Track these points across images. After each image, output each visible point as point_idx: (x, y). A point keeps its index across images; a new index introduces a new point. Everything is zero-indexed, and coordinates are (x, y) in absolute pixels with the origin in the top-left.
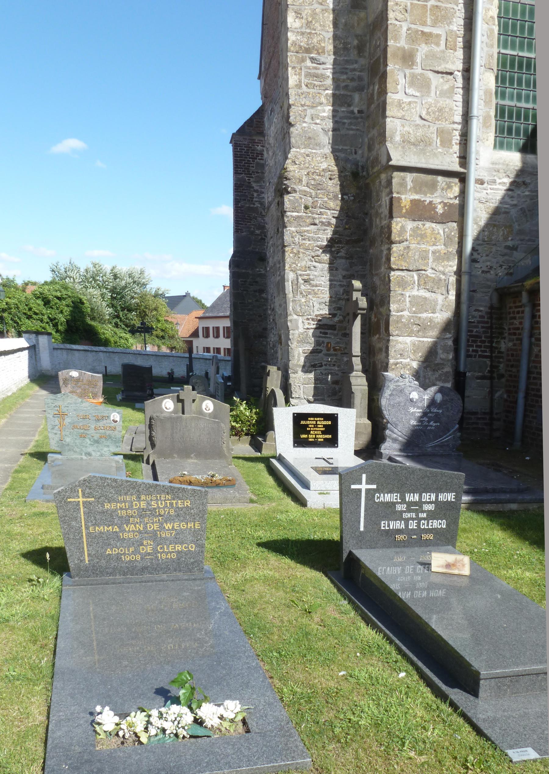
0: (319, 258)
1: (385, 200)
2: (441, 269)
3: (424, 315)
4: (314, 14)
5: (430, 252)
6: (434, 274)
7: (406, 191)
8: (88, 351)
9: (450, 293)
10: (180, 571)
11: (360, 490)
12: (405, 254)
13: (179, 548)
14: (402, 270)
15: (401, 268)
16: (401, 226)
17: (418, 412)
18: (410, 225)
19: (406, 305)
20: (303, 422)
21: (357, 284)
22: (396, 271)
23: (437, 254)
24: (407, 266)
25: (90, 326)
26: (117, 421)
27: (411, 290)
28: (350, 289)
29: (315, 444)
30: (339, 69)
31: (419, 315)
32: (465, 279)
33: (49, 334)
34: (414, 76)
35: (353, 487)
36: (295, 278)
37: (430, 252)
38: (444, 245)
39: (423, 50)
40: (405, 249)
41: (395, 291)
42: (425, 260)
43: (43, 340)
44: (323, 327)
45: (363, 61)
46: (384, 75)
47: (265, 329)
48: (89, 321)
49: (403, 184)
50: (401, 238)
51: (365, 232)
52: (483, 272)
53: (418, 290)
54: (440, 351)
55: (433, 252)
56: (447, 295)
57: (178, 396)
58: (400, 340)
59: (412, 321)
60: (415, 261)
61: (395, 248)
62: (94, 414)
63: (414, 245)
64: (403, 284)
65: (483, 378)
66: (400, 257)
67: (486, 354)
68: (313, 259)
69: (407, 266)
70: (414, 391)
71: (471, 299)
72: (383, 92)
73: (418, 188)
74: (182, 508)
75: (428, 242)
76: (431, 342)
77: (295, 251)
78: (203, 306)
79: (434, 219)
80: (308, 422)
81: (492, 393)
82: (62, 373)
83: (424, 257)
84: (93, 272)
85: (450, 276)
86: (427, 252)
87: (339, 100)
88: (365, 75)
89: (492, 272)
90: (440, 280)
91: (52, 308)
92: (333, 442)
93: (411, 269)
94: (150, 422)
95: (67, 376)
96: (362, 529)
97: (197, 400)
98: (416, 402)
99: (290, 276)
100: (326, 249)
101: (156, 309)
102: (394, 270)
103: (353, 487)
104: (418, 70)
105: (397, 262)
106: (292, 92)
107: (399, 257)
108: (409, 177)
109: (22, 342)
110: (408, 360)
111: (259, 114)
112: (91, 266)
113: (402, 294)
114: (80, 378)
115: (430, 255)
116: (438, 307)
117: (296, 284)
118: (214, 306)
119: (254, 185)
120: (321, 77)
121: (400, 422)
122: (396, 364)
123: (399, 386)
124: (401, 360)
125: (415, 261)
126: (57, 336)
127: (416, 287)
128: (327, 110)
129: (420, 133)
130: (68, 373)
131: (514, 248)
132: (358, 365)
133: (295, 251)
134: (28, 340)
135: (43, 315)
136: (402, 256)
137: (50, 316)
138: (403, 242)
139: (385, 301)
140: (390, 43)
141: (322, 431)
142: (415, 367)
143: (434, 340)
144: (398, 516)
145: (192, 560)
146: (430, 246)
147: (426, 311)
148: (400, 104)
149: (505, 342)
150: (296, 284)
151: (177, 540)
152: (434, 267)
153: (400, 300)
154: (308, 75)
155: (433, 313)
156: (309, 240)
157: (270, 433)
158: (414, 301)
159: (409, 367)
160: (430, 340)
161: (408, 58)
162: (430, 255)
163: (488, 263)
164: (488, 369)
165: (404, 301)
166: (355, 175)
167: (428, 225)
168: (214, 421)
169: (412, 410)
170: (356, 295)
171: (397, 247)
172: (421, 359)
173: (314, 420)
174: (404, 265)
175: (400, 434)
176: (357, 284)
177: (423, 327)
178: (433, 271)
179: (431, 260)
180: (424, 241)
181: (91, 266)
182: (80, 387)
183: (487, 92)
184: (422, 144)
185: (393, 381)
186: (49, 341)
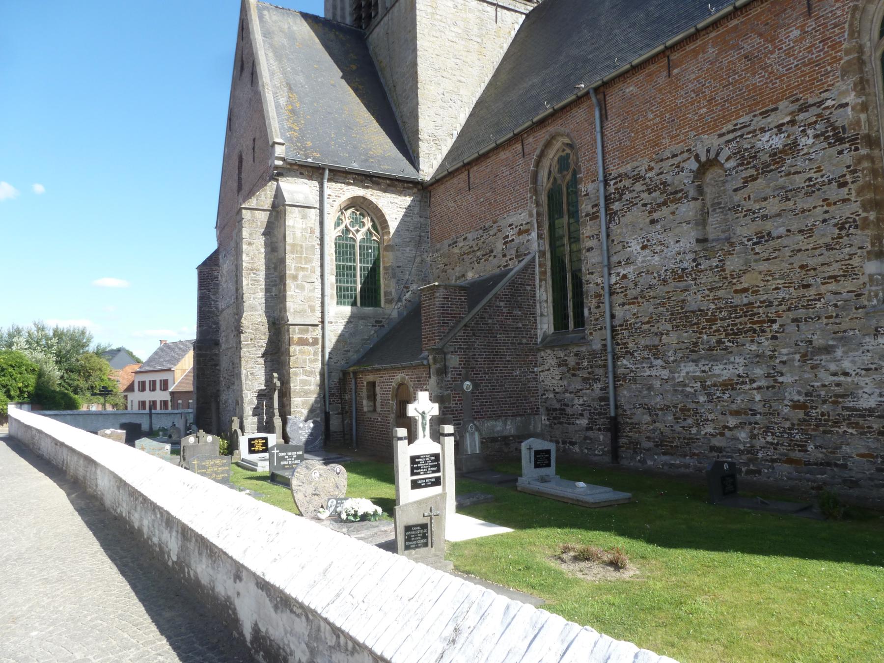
1: (287, 337)
4: (255, 255)
7: (295, 334)
16: (294, 349)
18: (298, 348)
21: (275, 375)
28: (272, 377)
29: (259, 452)
30: (267, 277)
32: (326, 367)
34: (297, 285)
39: (301, 274)
41: (293, 377)
44: (261, 395)
45: (276, 274)
46: (285, 284)
47: (218, 391)
49: (294, 331)
51: (279, 349)
61: (292, 358)
64: (296, 374)
65: (338, 414)
71: (329, 376)
72: (285, 291)
73: (301, 332)
78: (138, 361)
79: (308, 344)
81: (343, 421)
83: (305, 362)
84: (30, 335)
87: (268, 290)
88: (277, 279)
92: (414, 460)
99: (244, 372)
101: (100, 370)
104: (299, 282)
106: (244, 288)
108: (297, 328)
111: (216, 253)
112: (34, 330)
117: (247, 376)
118: (150, 361)
119: (212, 296)
120: (259, 281)
129: (301, 307)
131: (348, 351)
139: (288, 382)
140: (287, 272)
144: (286, 460)
148: (292, 296)
150: (247, 376)
151: (222, 473)
154: (252, 280)
157: (236, 452)
161: (295, 278)
166: (274, 323)
167: (306, 347)
170: (275, 380)
176: (275, 375)
177: (307, 393)
181: (34, 330)
183: (332, 284)
184: (301, 312)
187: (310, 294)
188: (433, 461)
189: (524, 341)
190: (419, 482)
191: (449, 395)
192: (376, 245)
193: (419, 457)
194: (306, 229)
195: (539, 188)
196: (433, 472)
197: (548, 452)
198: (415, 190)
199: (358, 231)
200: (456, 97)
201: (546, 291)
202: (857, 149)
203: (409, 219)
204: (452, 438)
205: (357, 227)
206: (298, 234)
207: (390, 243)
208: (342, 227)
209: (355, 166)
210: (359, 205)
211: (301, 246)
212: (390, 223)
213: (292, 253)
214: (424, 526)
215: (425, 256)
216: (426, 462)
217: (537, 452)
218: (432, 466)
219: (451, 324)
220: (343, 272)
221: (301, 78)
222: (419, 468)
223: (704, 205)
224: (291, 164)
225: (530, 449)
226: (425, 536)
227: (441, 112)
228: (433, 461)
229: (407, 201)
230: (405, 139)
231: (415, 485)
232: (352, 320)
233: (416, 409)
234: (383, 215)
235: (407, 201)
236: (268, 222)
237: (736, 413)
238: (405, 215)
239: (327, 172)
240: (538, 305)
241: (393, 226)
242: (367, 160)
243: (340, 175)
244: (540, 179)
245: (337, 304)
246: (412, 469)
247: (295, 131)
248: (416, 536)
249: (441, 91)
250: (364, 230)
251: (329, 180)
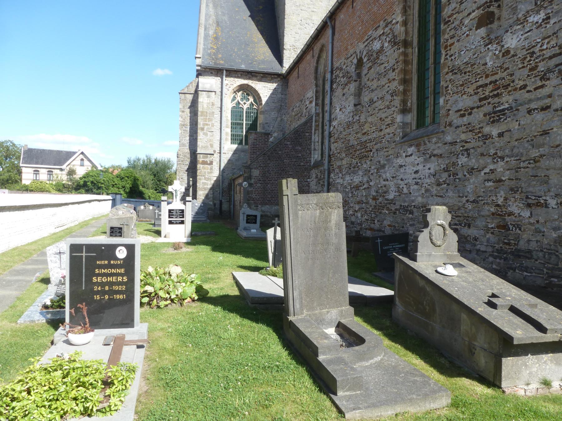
18: (202, 166)
33: (121, 194)
39: (206, 127)
43: (118, 197)
48: (141, 188)
49: (200, 157)
64: (200, 179)
72: (197, 136)
73: (203, 158)
92: (170, 211)
100: (187, 171)
104: (205, 131)
108: (201, 155)
109: (110, 197)
126: (125, 195)
128: (188, 138)
134: (112, 197)
148: (201, 139)
158: (203, 183)
161: (203, 129)
176: (191, 179)
177: (205, 189)
181: (146, 159)
184: (206, 147)
186: (121, 197)
187: (211, 138)
189: (302, 164)
191: (252, 191)
192: (256, 111)
193: (173, 210)
194: (209, 103)
195: (319, 76)
196: (180, 218)
197: (256, 216)
198: (279, 79)
199: (245, 103)
200: (310, 21)
201: (318, 136)
202: (399, 49)
203: (275, 96)
205: (245, 101)
206: (205, 106)
207: (262, 110)
208: (236, 101)
209: (243, 67)
210: (246, 90)
211: (207, 112)
212: (262, 99)
213: (202, 116)
214: (121, 228)
215: (283, 117)
216: (176, 213)
217: (248, 216)
219: (258, 153)
220: (235, 125)
221: (226, 18)
223: (360, 84)
224: (205, 68)
225: (244, 213)
226: (120, 232)
227: (299, 31)
229: (273, 86)
230: (277, 48)
231: (171, 222)
232: (236, 152)
234: (259, 94)
235: (273, 86)
236: (193, 100)
237: (359, 203)
238: (272, 94)
239: (225, 71)
240: (313, 144)
241: (264, 100)
242: (251, 63)
243: (232, 73)
244: (319, 71)
245: (231, 143)
246: (169, 215)
247: (214, 49)
248: (116, 231)
249: (300, 19)
250: (249, 103)
251: (227, 76)
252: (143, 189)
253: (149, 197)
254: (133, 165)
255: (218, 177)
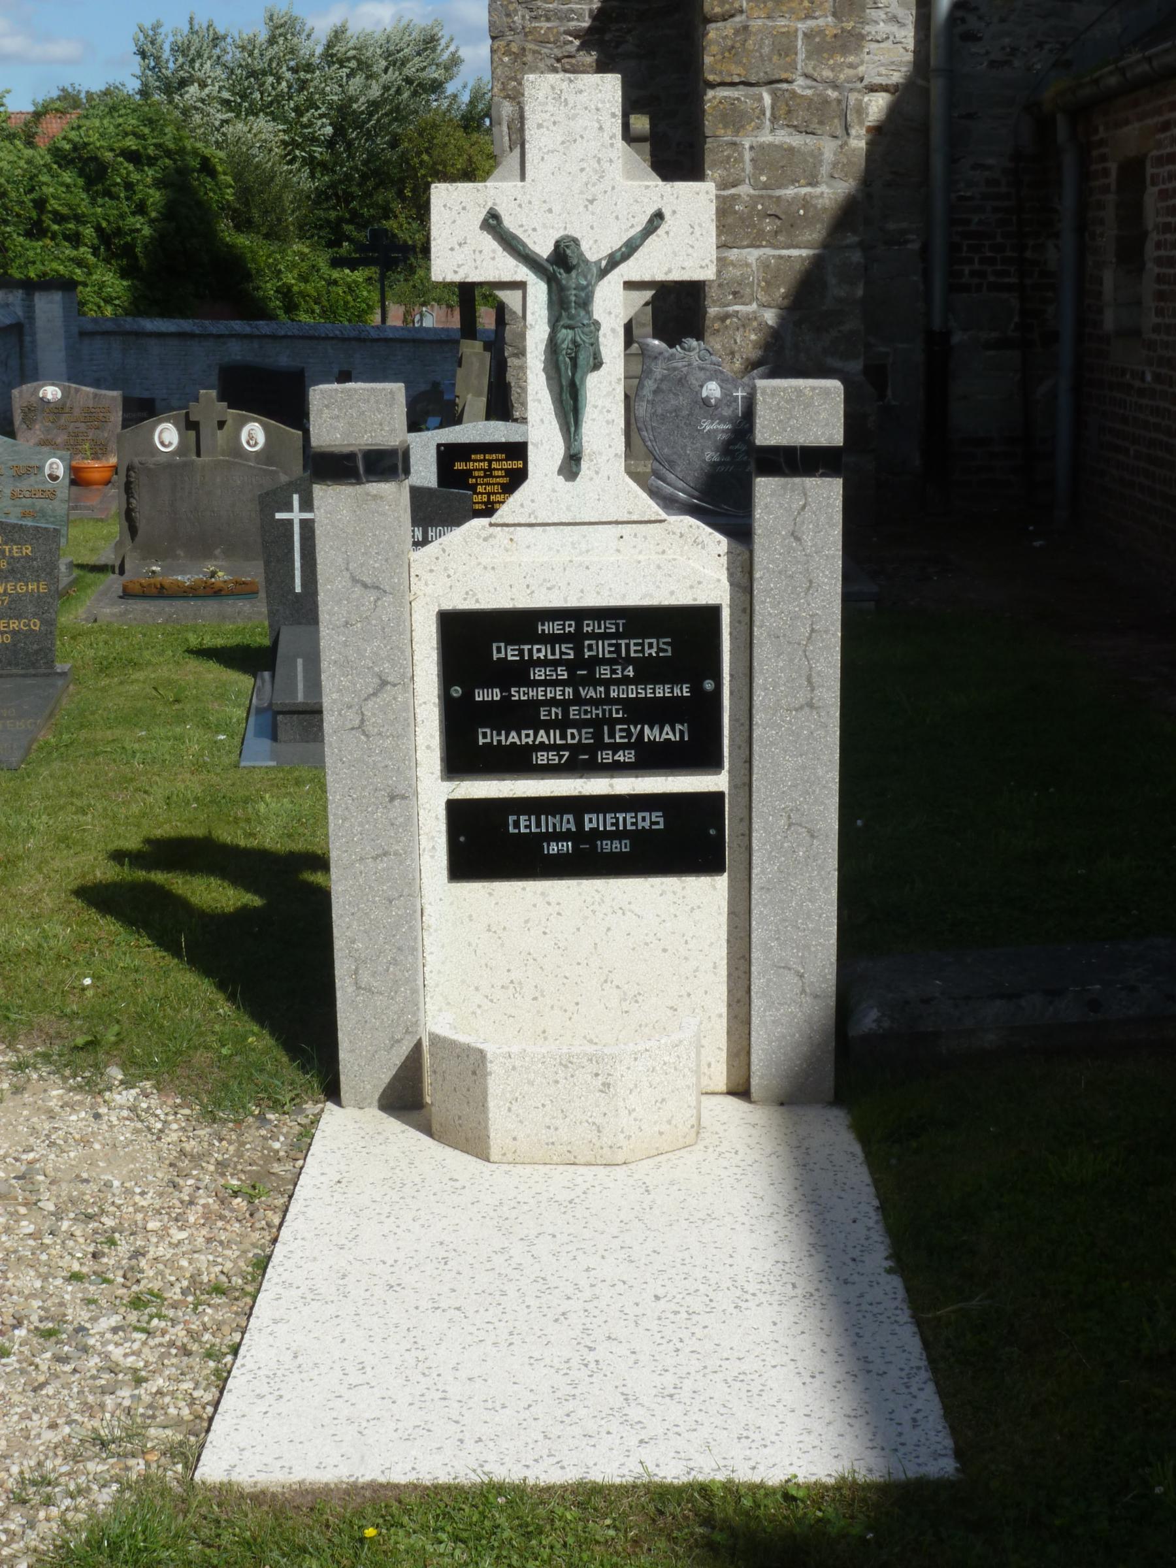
0: (573, 61)
2: (827, 74)
3: (789, 192)
5: (800, 35)
6: (810, 88)
8: (190, 336)
9: (853, 132)
10: (17, 665)
11: (290, 522)
12: (738, 45)
13: (14, 625)
14: (733, 84)
15: (728, 80)
17: (723, 431)
19: (743, 170)
20: (459, 466)
22: (718, 89)
23: (817, 40)
24: (743, 72)
25: (231, 247)
26: (57, 477)
27: (755, 133)
31: (778, 193)
32: (937, 87)
35: (278, 516)
36: (517, 116)
37: (800, 35)
38: (834, 14)
40: (737, 32)
42: (787, 55)
48: (226, 231)
50: (727, 7)
52: (993, 64)
53: (773, 130)
54: (832, 281)
55: (805, 34)
56: (845, 138)
57: (187, 414)
58: (732, 258)
59: (760, 207)
60: (763, 60)
61: (714, 32)
62: (11, 464)
63: (760, 22)
64: (736, 119)
66: (727, 54)
67: (1007, 280)
68: (558, 65)
69: (743, 72)
70: (711, 379)
74: (19, 558)
75: (792, 11)
76: (808, 257)
77: (514, 48)
80: (471, 465)
82: (21, 392)
83: (784, 47)
85: (851, 90)
86: (791, 35)
89: (1016, 63)
90: (826, 102)
91: (112, 196)
93: (753, 79)
94: (128, 476)
95: (33, 399)
96: (298, 589)
97: (229, 422)
98: (716, 407)
102: (713, 86)
103: (278, 516)
105: (718, 67)
107: (722, 54)
110: (754, 306)
113: (735, 144)
114: (64, 404)
115: (800, 43)
116: (824, 170)
121: (680, 456)
122: (723, 318)
123: (675, 369)
124: (737, 308)
125: (763, 60)
127: (768, 123)
130: (36, 391)
132: (644, 325)
133: (514, 48)
135: (79, 219)
136: (731, 52)
137: (104, 224)
138: (732, 16)
141: (502, 485)
142: (770, 323)
143: (816, 251)
145: (35, 647)
146: (800, 19)
147: (794, 181)
149: (1057, 246)
152: (810, 70)
153: (729, 157)
155: (810, 184)
156: (548, 20)
158: (765, 157)
159: (755, 324)
160: (804, 253)
162: (800, 43)
163: (1007, 41)
164: (1016, 319)
165: (740, 160)
168: (265, 470)
169: (707, 426)
171: (717, 29)
172: (786, 303)
173: (484, 460)
174: (737, 72)
175: (681, 484)
178: (809, 82)
179: (801, 56)
180: (784, 9)
182: (64, 428)
185: (661, 357)
188: (648, 671)
190: (525, 824)
193: (520, 624)
204: (826, 495)
216: (582, 670)
218: (640, 712)
222: (523, 715)
228: (648, 671)
231: (485, 847)
233: (493, 223)
252: (242, 240)
253: (286, 293)
254: (169, 74)
255: (908, 98)
